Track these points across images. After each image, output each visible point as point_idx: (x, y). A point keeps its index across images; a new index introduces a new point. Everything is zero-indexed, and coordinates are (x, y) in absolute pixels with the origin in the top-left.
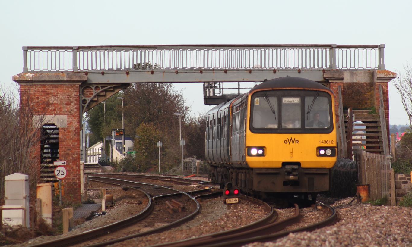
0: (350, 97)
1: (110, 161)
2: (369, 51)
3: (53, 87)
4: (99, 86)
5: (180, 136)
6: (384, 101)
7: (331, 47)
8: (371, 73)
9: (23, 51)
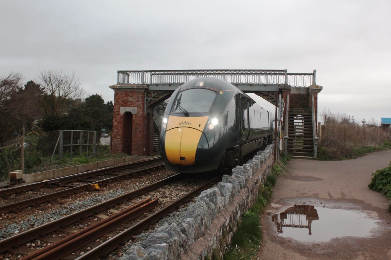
1: (246, 126)
2: (307, 76)
5: (85, 131)
8: (308, 89)
9: (117, 73)
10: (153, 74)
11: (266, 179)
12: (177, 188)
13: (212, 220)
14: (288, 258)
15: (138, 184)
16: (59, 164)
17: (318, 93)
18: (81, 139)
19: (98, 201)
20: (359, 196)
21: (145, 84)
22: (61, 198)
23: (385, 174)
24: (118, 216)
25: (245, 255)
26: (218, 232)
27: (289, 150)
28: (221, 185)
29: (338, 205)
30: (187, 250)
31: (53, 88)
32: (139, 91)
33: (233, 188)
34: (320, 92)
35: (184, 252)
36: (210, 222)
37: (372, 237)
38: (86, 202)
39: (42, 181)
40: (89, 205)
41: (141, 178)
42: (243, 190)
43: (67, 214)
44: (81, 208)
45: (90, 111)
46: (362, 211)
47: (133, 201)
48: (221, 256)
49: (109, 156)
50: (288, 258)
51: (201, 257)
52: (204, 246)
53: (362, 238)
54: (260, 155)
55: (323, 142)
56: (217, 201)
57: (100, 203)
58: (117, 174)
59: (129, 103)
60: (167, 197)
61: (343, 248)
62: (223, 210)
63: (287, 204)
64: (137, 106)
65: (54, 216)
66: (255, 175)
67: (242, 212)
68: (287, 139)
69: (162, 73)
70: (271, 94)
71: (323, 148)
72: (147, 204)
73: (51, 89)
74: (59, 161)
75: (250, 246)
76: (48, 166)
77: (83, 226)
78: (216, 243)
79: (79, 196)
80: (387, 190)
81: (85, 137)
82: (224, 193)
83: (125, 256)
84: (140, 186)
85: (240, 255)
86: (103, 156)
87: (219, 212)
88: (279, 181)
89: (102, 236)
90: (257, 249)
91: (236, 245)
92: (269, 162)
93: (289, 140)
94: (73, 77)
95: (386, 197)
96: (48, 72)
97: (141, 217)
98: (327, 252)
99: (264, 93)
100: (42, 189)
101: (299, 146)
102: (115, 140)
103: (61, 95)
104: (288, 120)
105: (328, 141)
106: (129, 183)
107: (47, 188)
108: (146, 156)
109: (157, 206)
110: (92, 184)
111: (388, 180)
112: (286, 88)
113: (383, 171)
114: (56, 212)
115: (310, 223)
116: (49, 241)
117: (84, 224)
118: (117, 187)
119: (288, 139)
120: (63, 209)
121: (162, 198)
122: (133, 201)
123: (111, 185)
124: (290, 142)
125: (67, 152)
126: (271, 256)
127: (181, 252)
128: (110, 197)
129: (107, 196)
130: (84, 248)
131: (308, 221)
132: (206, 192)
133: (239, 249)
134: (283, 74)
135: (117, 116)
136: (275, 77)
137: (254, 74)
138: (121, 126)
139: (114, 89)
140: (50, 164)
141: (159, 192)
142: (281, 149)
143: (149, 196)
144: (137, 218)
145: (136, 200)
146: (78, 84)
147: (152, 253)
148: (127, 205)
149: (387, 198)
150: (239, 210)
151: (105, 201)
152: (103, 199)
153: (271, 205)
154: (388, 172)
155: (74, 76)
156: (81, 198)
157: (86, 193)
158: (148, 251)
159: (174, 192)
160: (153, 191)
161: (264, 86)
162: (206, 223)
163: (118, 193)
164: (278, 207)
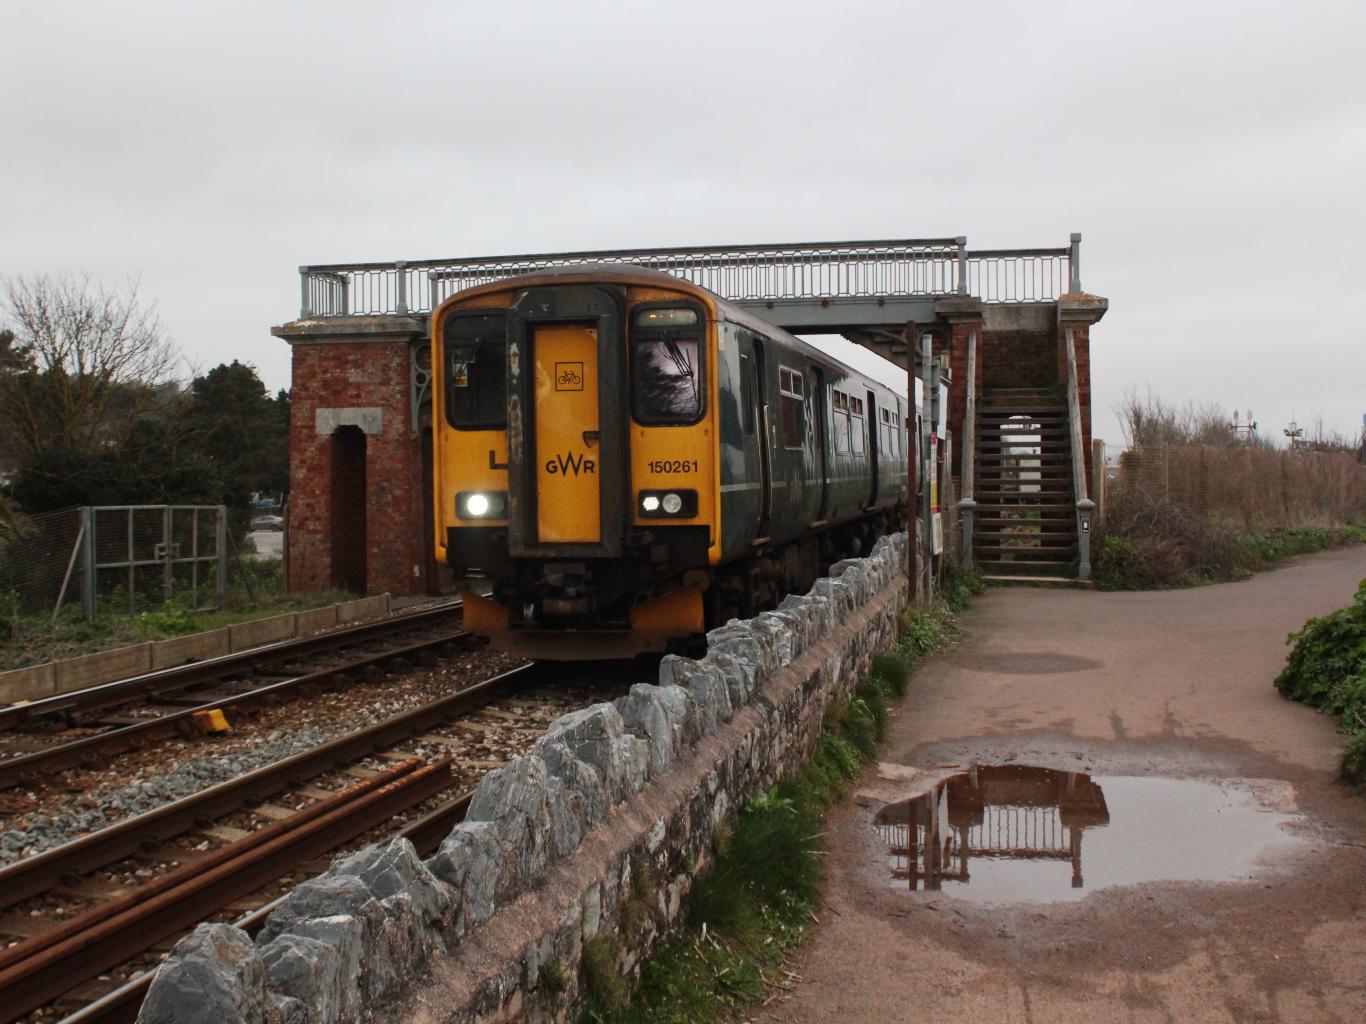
0: (1005, 363)
2: (1047, 260)
8: (1050, 310)
9: (300, 275)
10: (440, 276)
11: (866, 670)
12: (533, 715)
13: (587, 828)
14: (911, 971)
15: (377, 705)
16: (83, 637)
17: (1092, 328)
18: (166, 536)
19: (218, 776)
20: (1233, 727)
21: (410, 316)
22: (74, 768)
23: (1335, 634)
24: (285, 829)
25: (737, 962)
26: (607, 873)
27: (979, 556)
28: (637, 695)
29: (1144, 760)
30: (461, 941)
31: (57, 345)
32: (389, 343)
33: (690, 705)
34: (1098, 319)
35: (444, 949)
36: (576, 837)
37: (1256, 881)
38: (169, 780)
39: (8, 705)
40: (179, 790)
41: (394, 681)
42: (747, 710)
43: (92, 829)
44: (149, 804)
45: (203, 427)
46: (1234, 783)
47: (352, 771)
48: (627, 969)
49: (282, 601)
50: (911, 971)
51: (525, 968)
52: (538, 927)
53: (1220, 885)
54: (840, 575)
55: (1114, 518)
56: (607, 755)
57: (221, 784)
58: (304, 670)
59: (349, 393)
60: (487, 751)
61: (1135, 927)
62: (641, 791)
63: (940, 764)
65: (40, 838)
66: (809, 654)
67: (738, 796)
68: (971, 513)
69: (474, 267)
71: (1115, 541)
72: (404, 780)
73: (49, 349)
74: (83, 627)
75: (764, 928)
76: (40, 646)
77: (149, 873)
78: (602, 916)
79: (150, 758)
80: (1344, 696)
81: (181, 529)
82: (648, 726)
83: (171, 963)
84: (388, 714)
85: (716, 963)
86: (257, 604)
87: (622, 796)
88: (922, 679)
89: (222, 910)
90: (792, 937)
91: (704, 925)
92: (886, 602)
93: (978, 513)
94: (132, 297)
95: (1340, 724)
96: (34, 281)
97: (377, 833)
98: (1070, 942)
99: (877, 334)
100: (6, 736)
101: (1025, 537)
102: (303, 537)
103: (88, 370)
104: (972, 437)
105: (1134, 513)
106: (343, 705)
107: (27, 732)
108: (425, 598)
109: (446, 788)
110: (197, 711)
111: (1348, 659)
112: (965, 310)
113: (1329, 622)
114: (51, 823)
115: (1076, 838)
116: (16, 933)
117: (155, 863)
118: (297, 719)
119: (975, 513)
120: (77, 812)
121: (467, 759)
122: (354, 771)
123: (276, 714)
124: (986, 520)
125: (115, 592)
126: (846, 964)
127: (431, 948)
128: (265, 760)
129: (254, 756)
130: (147, 956)
131: (1067, 832)
132: (568, 720)
133: (713, 938)
134: (948, 256)
135: (303, 445)
136: (798, 270)
137: (853, 257)
138: (320, 483)
140: (49, 641)
141: (459, 734)
142: (938, 549)
143: (420, 751)
144: (361, 835)
145: (365, 767)
146: (154, 326)
147: (290, 951)
148: (330, 787)
149: (1340, 730)
150: (718, 789)
151: (241, 776)
152: (236, 766)
153: (880, 768)
154: (1347, 627)
155: (134, 295)
156: (151, 769)
157: (175, 747)
158: (277, 942)
159: (519, 731)
160: (434, 731)
161: (877, 306)
162: (551, 838)
163: (299, 744)
164: (906, 775)
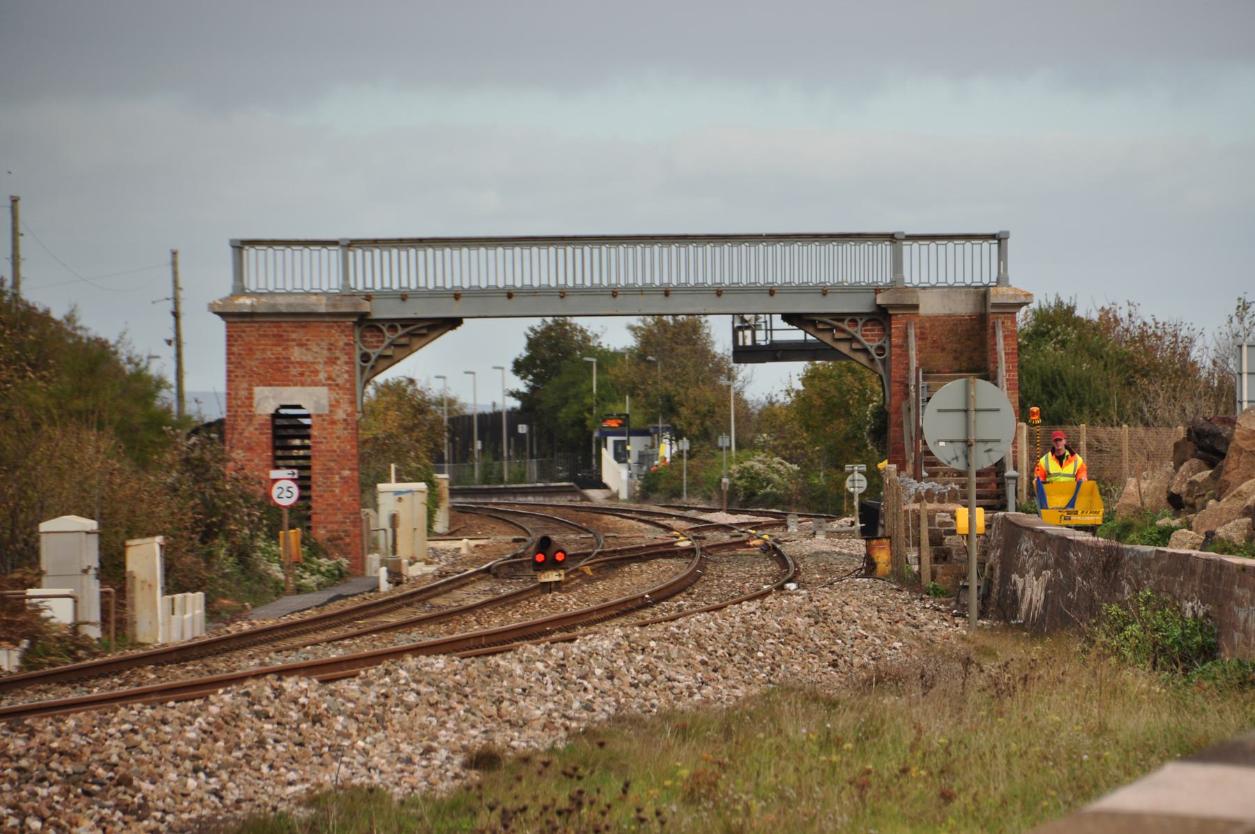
2: (977, 245)
3: (296, 327)
4: (398, 325)
6: (1006, 354)
7: (891, 238)
8: (982, 294)
64: (329, 382)
70: (846, 322)
99: (820, 322)
139: (222, 315)
